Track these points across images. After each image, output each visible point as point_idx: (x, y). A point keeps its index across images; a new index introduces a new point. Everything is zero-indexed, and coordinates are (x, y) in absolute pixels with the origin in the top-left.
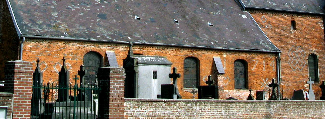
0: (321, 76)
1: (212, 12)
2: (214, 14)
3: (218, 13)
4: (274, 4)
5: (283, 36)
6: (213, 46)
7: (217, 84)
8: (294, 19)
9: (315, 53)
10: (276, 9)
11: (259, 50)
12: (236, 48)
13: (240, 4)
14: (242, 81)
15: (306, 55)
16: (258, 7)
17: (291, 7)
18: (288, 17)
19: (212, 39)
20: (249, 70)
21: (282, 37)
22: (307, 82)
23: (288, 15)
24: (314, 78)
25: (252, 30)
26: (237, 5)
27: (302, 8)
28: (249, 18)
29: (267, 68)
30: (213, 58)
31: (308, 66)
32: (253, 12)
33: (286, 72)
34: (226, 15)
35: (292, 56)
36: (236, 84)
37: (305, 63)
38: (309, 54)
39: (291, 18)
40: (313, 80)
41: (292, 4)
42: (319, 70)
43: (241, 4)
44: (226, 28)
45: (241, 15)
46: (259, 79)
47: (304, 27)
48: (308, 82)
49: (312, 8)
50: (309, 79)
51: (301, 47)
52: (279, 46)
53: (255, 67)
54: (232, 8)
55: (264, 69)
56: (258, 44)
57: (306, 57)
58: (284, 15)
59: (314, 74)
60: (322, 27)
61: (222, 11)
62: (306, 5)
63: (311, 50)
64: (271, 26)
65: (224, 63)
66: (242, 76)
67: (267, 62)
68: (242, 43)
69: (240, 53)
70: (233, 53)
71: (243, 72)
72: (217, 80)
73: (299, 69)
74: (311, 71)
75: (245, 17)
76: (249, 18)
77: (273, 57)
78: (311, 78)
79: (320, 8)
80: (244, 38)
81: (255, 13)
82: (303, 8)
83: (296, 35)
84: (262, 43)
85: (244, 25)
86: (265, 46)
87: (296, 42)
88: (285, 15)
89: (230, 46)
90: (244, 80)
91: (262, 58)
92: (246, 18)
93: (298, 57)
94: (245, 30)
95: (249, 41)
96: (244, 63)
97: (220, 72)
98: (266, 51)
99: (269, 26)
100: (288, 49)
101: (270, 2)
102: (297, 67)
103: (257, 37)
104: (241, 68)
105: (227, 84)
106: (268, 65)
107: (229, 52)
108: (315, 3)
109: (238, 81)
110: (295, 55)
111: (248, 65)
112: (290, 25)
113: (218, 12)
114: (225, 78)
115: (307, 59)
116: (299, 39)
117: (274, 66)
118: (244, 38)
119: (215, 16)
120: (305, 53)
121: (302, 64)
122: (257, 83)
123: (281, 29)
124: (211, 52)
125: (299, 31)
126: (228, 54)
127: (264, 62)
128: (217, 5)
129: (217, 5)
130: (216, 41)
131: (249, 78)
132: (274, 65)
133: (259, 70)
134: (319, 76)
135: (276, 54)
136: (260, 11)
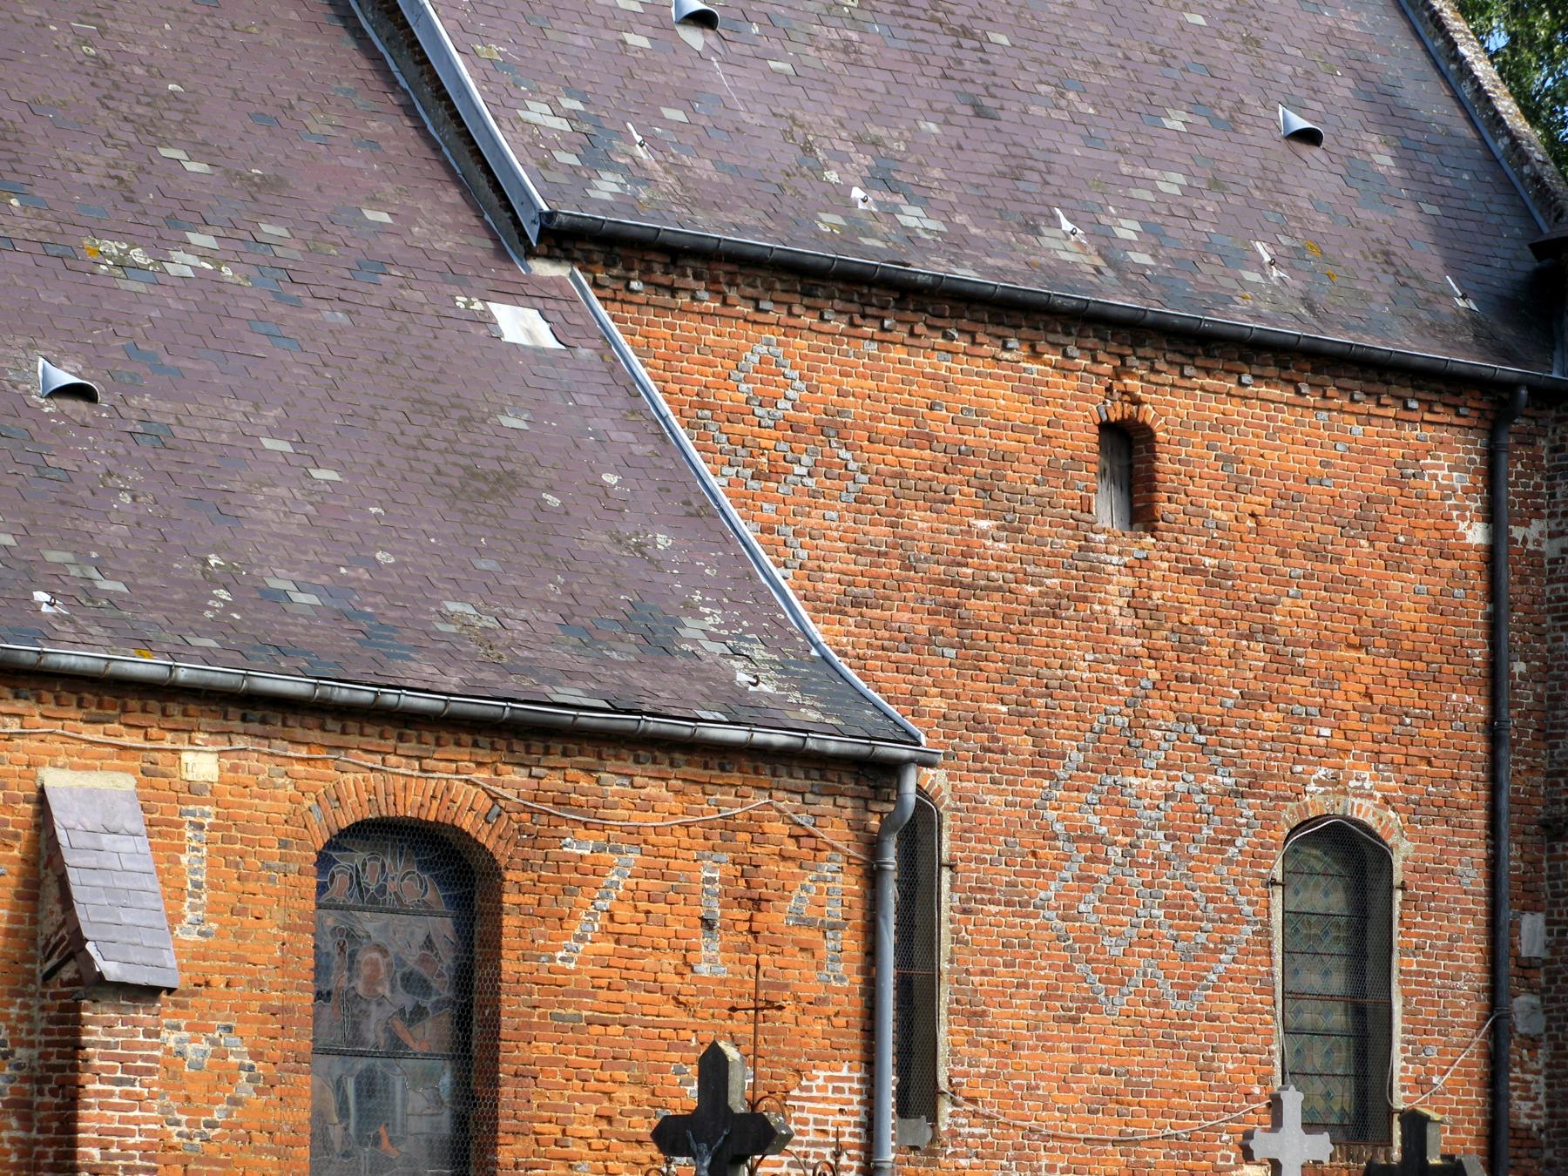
0: (1422, 1084)
1: (111, 247)
2: (137, 267)
3: (182, 264)
4: (912, 217)
5: (999, 589)
6: (44, 631)
7: (75, 1118)
8: (1138, 402)
9: (1370, 820)
10: (930, 266)
11: (652, 725)
12: (354, 672)
13: (483, 181)
14: (418, 1100)
15: (1263, 833)
16: (708, 226)
17: (1111, 264)
18: (1064, 371)
19: (53, 556)
20: (509, 966)
21: (978, 607)
22: (1249, 1135)
23: (1072, 350)
24: (1342, 1097)
25: (604, 486)
26: (452, 196)
27: (1240, 280)
28: (584, 353)
29: (746, 949)
30: (42, 790)
31: (1278, 958)
32: (635, 285)
33: (1010, 1018)
34: (297, 292)
35: (1099, 839)
36: (336, 1133)
37: (1248, 929)
38: (1297, 821)
39: (1109, 389)
40: (1334, 1120)
41: (1127, 230)
42: (1410, 1014)
43: (497, 187)
44: (268, 443)
45: (478, 306)
46: (640, 1083)
47: (1259, 510)
48: (1263, 1145)
49: (1366, 298)
50: (1275, 1104)
51: (1200, 731)
52: (940, 704)
53: (587, 922)
54: (385, 218)
55: (712, 959)
56: (658, 641)
57: (1256, 859)
58: (1024, 351)
59: (1341, 1060)
60: (1462, 526)
61: (240, 242)
62: (1291, 259)
63: (1321, 772)
64: (852, 466)
65: (184, 859)
66: (432, 1034)
67: (748, 869)
68: (452, 629)
69: (404, 748)
70: (315, 735)
71: (443, 989)
72: (75, 1068)
73: (1166, 989)
74: (1307, 1019)
75: (529, 333)
76: (584, 353)
77: (835, 819)
78: (1300, 1096)
79: (1461, 303)
80: (483, 564)
81: (666, 298)
82: (1259, 295)
83: (1156, 595)
84: (712, 637)
85: (510, 422)
86: (735, 674)
87: (1154, 675)
88: (1035, 355)
89: (281, 652)
90: (446, 1080)
91: (687, 826)
92: (549, 342)
93: (1167, 848)
94: (506, 483)
95: (544, 604)
96: (457, 867)
97: (111, 969)
98: (737, 734)
99: (826, 467)
100: (1044, 759)
101: (857, 193)
102: (1139, 964)
103: (656, 564)
104: (410, 925)
105: (211, 1125)
106: (757, 903)
107: (255, 727)
108: (1398, 247)
109: (369, 1087)
110: (1128, 828)
111: (509, 899)
112: (1087, 475)
113: (186, 246)
114: (189, 1048)
115: (1274, 883)
116: (1188, 643)
117: (833, 927)
118: (483, 564)
119: (141, 287)
120: (1248, 809)
121: (1202, 938)
122: (609, 1120)
123: (978, 516)
124: (20, 706)
125: (1193, 544)
126: (240, 743)
127: (714, 870)
128: (192, 167)
129: (192, 167)
130: (105, 585)
131: (512, 1056)
132: (835, 911)
133: (649, 962)
134: (1396, 1084)
135: (874, 774)
136: (730, 284)
